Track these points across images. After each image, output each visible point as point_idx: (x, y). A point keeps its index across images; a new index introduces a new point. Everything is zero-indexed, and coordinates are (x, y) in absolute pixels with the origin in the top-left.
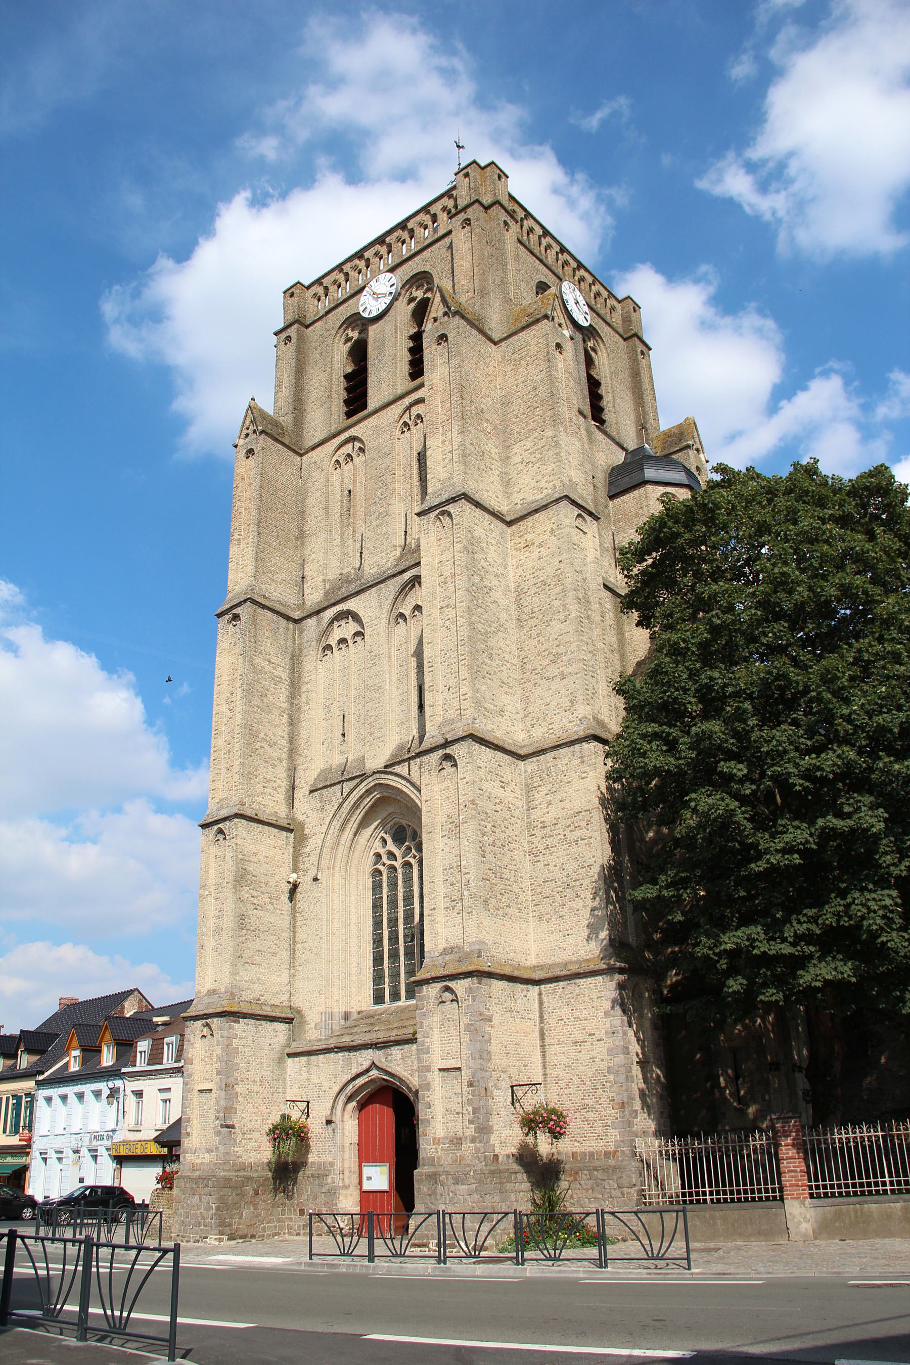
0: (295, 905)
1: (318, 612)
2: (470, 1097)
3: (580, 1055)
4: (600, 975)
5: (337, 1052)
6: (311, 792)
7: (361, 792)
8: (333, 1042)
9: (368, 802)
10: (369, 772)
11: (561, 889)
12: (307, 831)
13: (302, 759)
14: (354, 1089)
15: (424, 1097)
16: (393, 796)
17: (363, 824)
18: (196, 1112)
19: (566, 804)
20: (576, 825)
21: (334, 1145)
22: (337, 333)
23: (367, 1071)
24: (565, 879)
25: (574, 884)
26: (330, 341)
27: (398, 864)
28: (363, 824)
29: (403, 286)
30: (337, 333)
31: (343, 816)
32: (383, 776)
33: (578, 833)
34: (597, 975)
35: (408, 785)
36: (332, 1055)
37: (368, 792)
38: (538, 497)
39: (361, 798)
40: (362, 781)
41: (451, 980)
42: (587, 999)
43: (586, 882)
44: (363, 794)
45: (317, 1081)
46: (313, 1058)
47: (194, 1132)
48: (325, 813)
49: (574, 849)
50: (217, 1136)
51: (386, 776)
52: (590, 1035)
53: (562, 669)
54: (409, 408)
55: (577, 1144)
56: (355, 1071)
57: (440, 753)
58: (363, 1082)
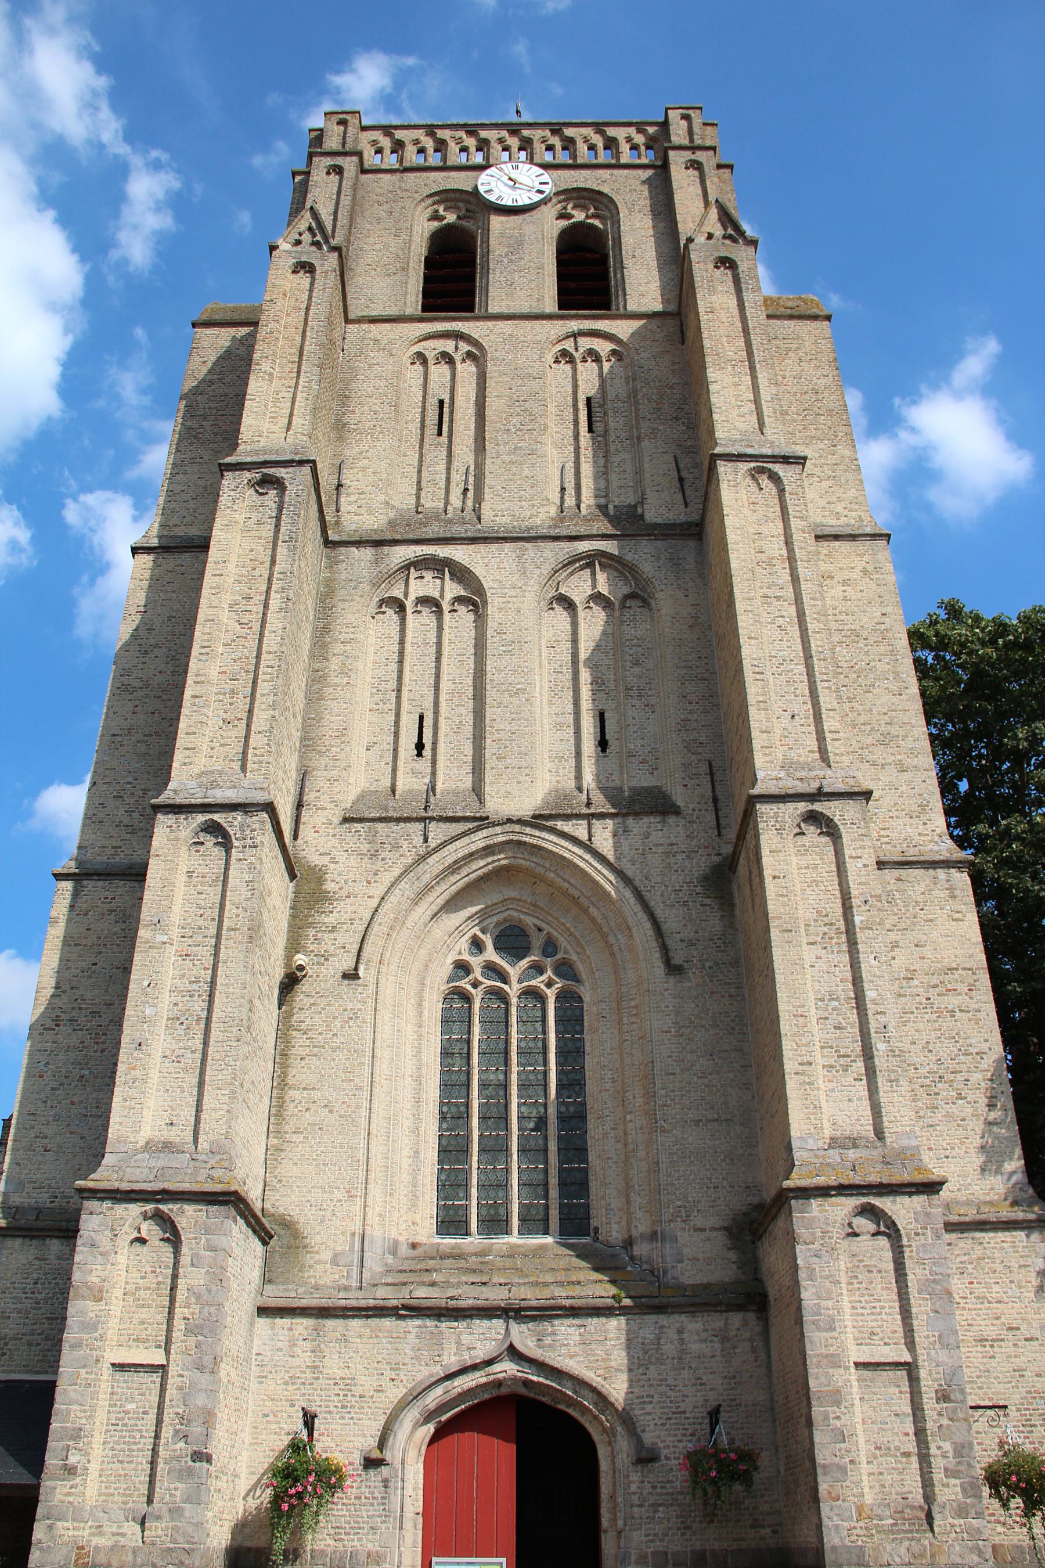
0: (288, 1016)
1: (378, 544)
2: (945, 1422)
3: (993, 1363)
4: (1022, 1229)
5: (403, 1317)
6: (346, 820)
7: (474, 848)
8: (392, 1297)
9: (480, 867)
10: (493, 817)
11: (927, 1082)
12: (329, 886)
13: (324, 761)
14: (448, 1397)
15: (826, 1417)
16: (539, 870)
17: (452, 905)
18: (101, 1416)
19: (928, 952)
20: (949, 987)
21: (386, 1514)
22: (423, 200)
23: (489, 1362)
24: (935, 1067)
25: (952, 1077)
26: (408, 203)
27: (513, 990)
28: (452, 905)
29: (557, 194)
30: (423, 200)
31: (426, 878)
32: (528, 830)
33: (953, 1001)
34: (1015, 1229)
35: (588, 857)
36: (387, 1323)
37: (488, 850)
38: (833, 522)
39: (471, 856)
40: (478, 829)
41: (880, 1194)
42: (998, 1267)
43: (976, 1077)
44: (477, 851)
45: (339, 1373)
46: (330, 1323)
47: (94, 1467)
48: (380, 863)
49: (947, 1023)
50: (180, 1479)
51: (537, 833)
52: (1010, 1329)
53: (899, 757)
54: (575, 335)
55: (1000, 1529)
56: (452, 1360)
57: (802, 807)
58: (466, 1387)
